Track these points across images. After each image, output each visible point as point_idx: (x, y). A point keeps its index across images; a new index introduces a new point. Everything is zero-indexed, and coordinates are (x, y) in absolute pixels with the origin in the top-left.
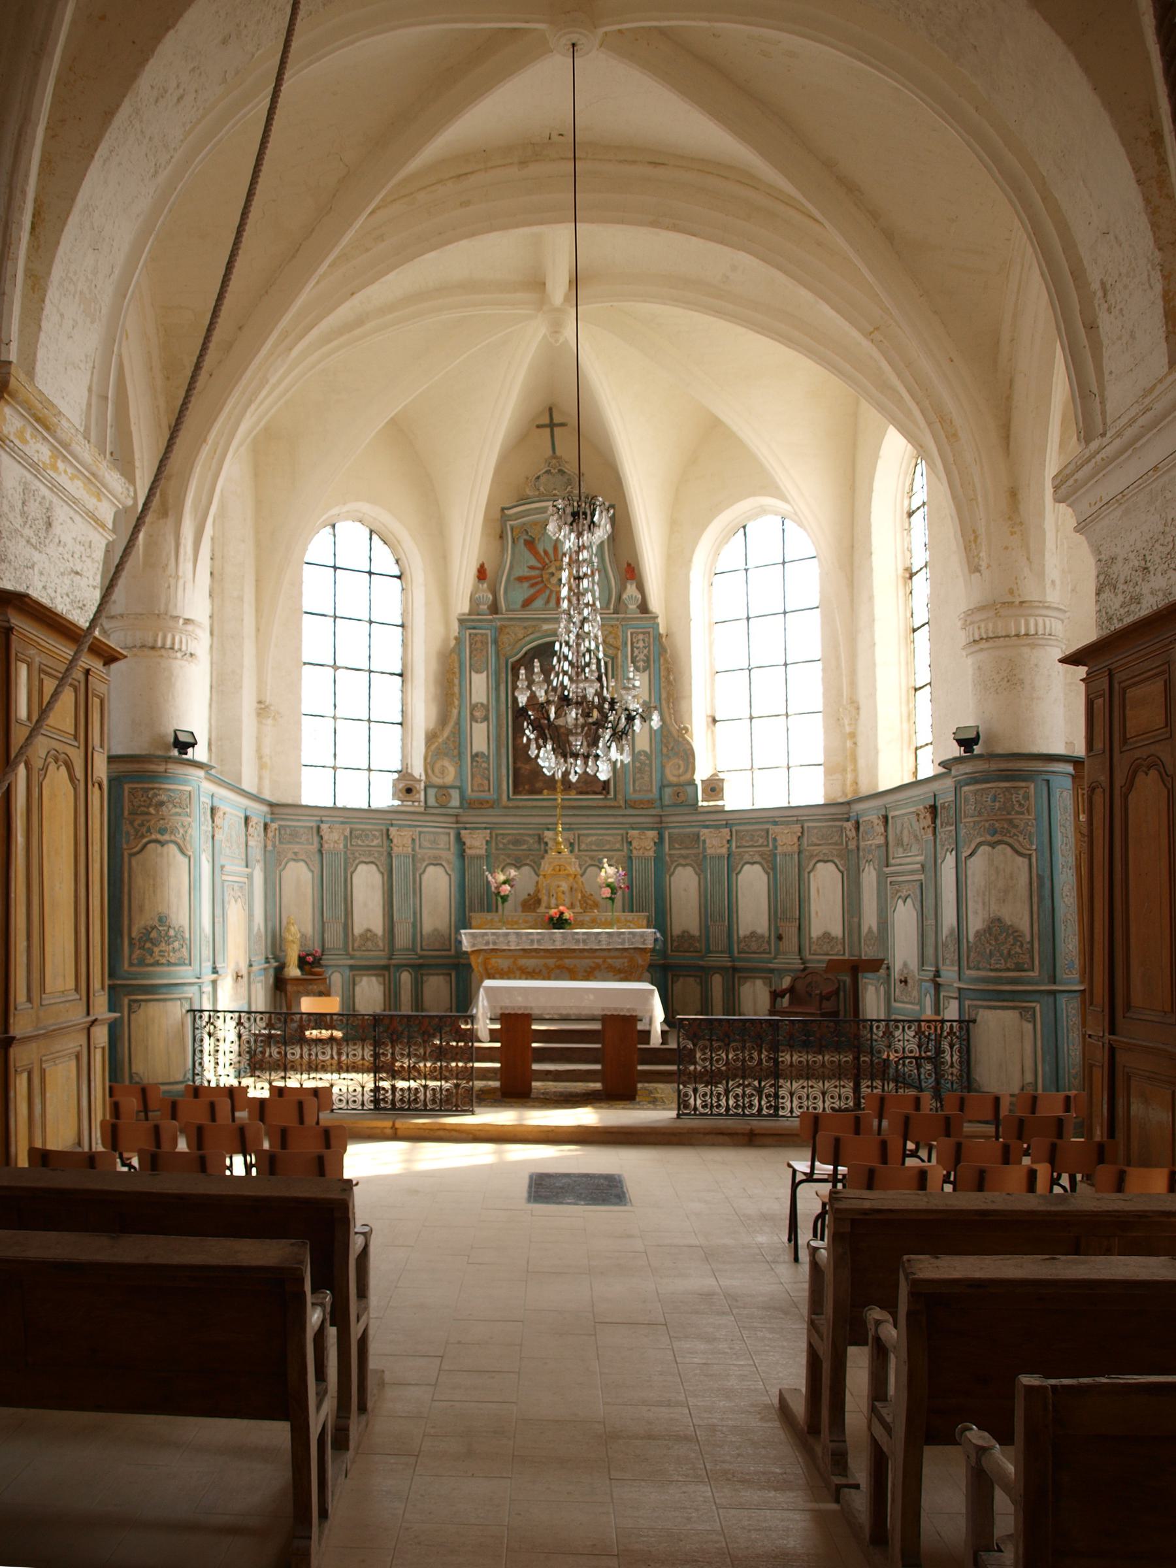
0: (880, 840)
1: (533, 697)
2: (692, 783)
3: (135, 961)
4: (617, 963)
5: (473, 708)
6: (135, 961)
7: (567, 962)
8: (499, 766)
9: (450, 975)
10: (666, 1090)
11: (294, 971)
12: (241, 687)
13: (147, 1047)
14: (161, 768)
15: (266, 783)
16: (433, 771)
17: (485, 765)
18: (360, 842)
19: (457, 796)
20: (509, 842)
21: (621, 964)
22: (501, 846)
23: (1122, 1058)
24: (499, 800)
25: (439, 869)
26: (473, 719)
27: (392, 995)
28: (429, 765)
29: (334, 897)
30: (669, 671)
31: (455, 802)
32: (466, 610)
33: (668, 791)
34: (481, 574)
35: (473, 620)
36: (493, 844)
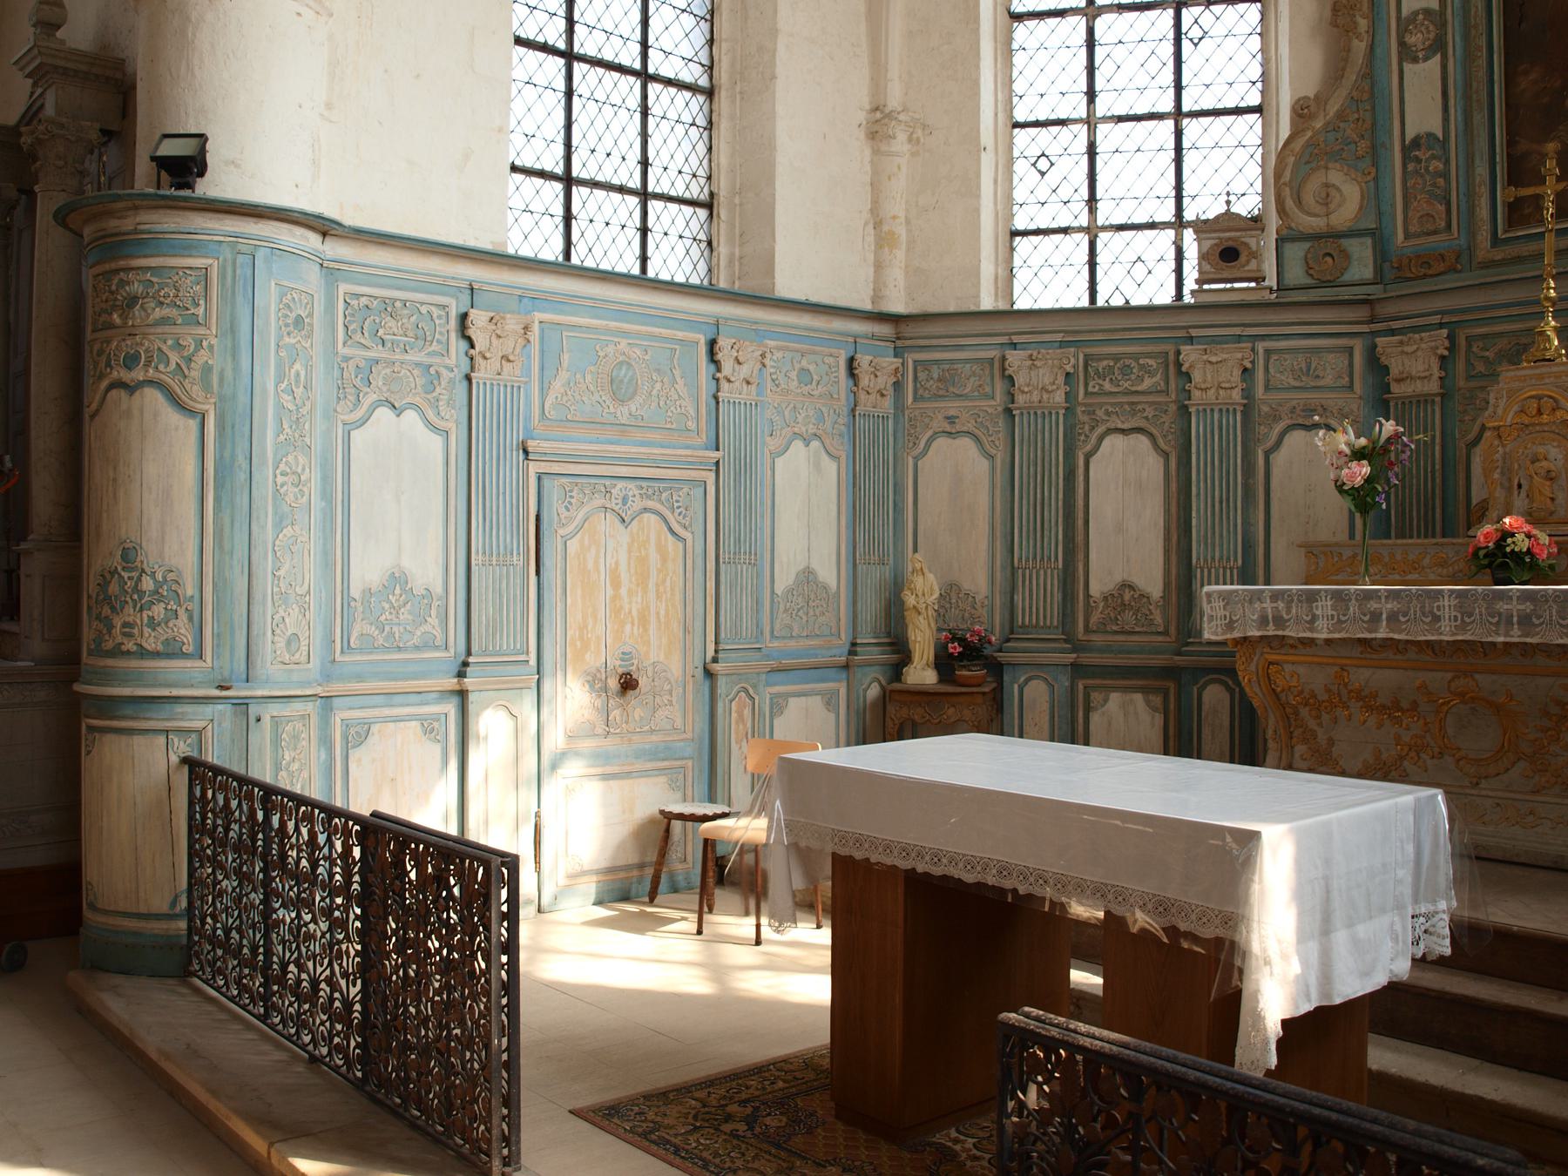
5: (1405, 25)
11: (922, 674)
12: (773, 77)
14: (127, 224)
15: (896, 276)
16: (1299, 202)
17: (1437, 165)
18: (1107, 386)
19: (1368, 253)
24: (1471, 249)
29: (1050, 512)
31: (1361, 263)
36: (1461, 366)
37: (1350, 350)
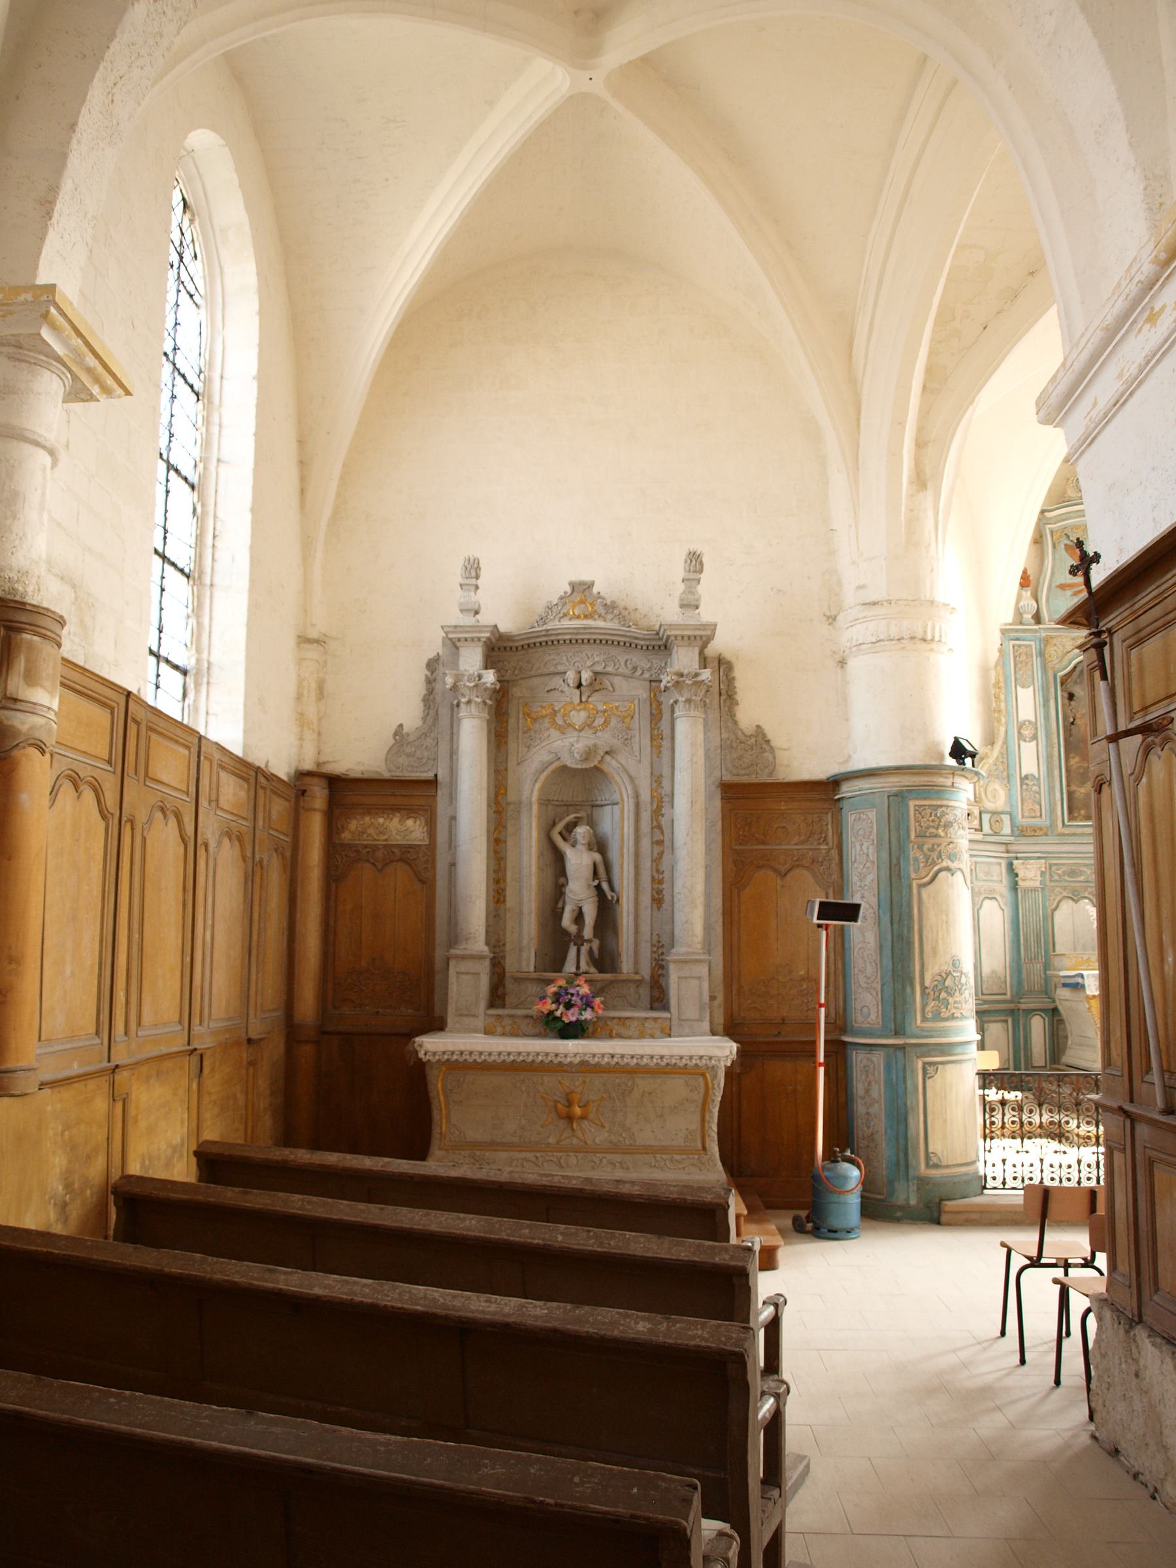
3: (930, 1015)
5: (1021, 726)
6: (930, 1015)
9: (1006, 1021)
13: (945, 1121)
14: (948, 782)
17: (1035, 788)
20: (1064, 873)
22: (1056, 877)
24: (1053, 825)
25: (994, 903)
31: (1007, 830)
32: (1010, 619)
34: (1025, 581)
35: (1017, 631)
36: (1047, 876)
37: (1000, 864)
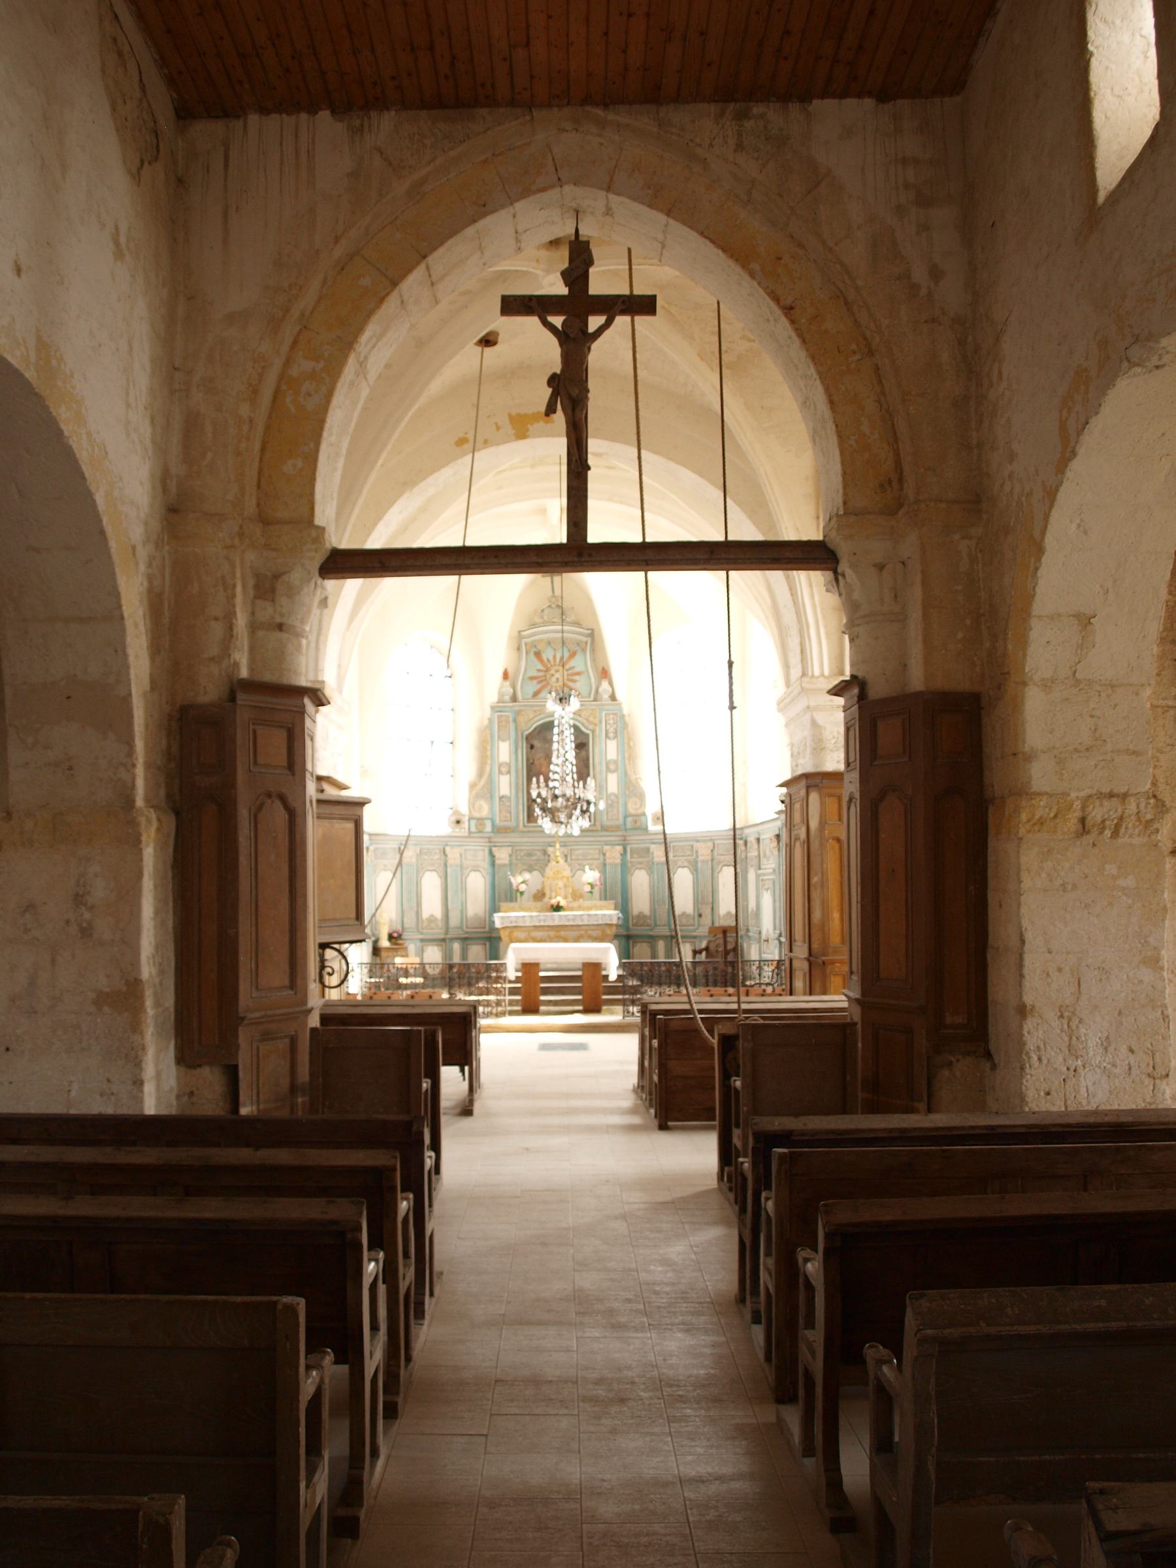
0: (756, 853)
1: (539, 795)
2: (644, 814)
4: (594, 934)
5: (500, 765)
7: (563, 933)
8: (517, 804)
10: (619, 1008)
21: (597, 933)
23: (794, 963)
24: (518, 825)
26: (500, 772)
27: (448, 954)
28: (472, 805)
30: (629, 739)
31: (488, 828)
33: (629, 820)
34: (506, 676)
